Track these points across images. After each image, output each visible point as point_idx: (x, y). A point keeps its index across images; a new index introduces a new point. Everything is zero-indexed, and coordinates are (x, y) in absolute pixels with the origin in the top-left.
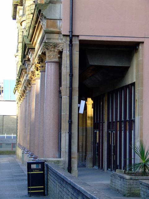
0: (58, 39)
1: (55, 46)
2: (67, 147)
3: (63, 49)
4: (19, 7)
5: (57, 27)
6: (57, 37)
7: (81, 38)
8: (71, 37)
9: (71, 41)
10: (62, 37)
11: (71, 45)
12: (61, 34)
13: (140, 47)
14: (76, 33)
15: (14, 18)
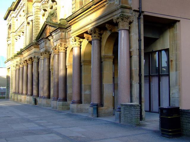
0: (129, 13)
1: (128, 18)
2: (138, 94)
3: (133, 21)
4: (12, 12)
5: (128, 4)
6: (129, 12)
7: (146, 13)
8: (140, 12)
9: (140, 15)
10: (132, 11)
11: (139, 18)
12: (132, 9)
13: (177, 24)
14: (143, 10)
15: (6, 19)
